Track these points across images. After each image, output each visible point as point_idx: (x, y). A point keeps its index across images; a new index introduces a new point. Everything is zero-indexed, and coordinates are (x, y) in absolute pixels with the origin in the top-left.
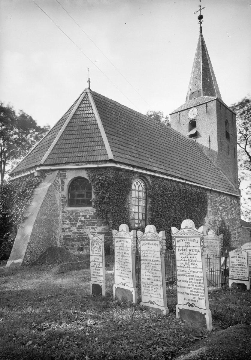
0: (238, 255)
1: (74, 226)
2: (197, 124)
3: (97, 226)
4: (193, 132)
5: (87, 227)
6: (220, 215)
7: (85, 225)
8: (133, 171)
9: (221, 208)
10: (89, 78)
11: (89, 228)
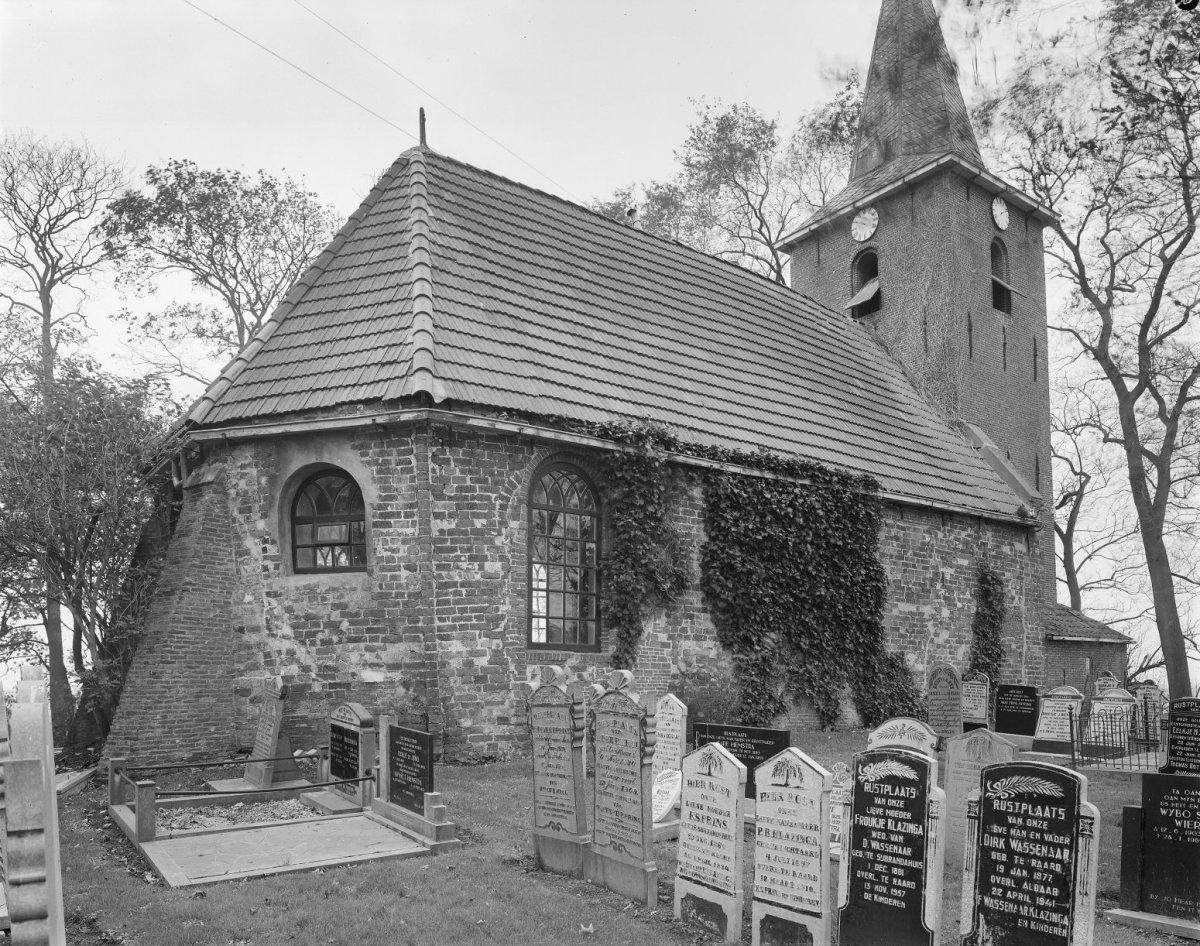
0: (710, 774)
1: (308, 643)
2: (881, 262)
3: (385, 640)
4: (867, 293)
5: (351, 646)
6: (945, 598)
7: (344, 640)
8: (519, 433)
9: (948, 572)
10: (422, 110)
11: (358, 649)
